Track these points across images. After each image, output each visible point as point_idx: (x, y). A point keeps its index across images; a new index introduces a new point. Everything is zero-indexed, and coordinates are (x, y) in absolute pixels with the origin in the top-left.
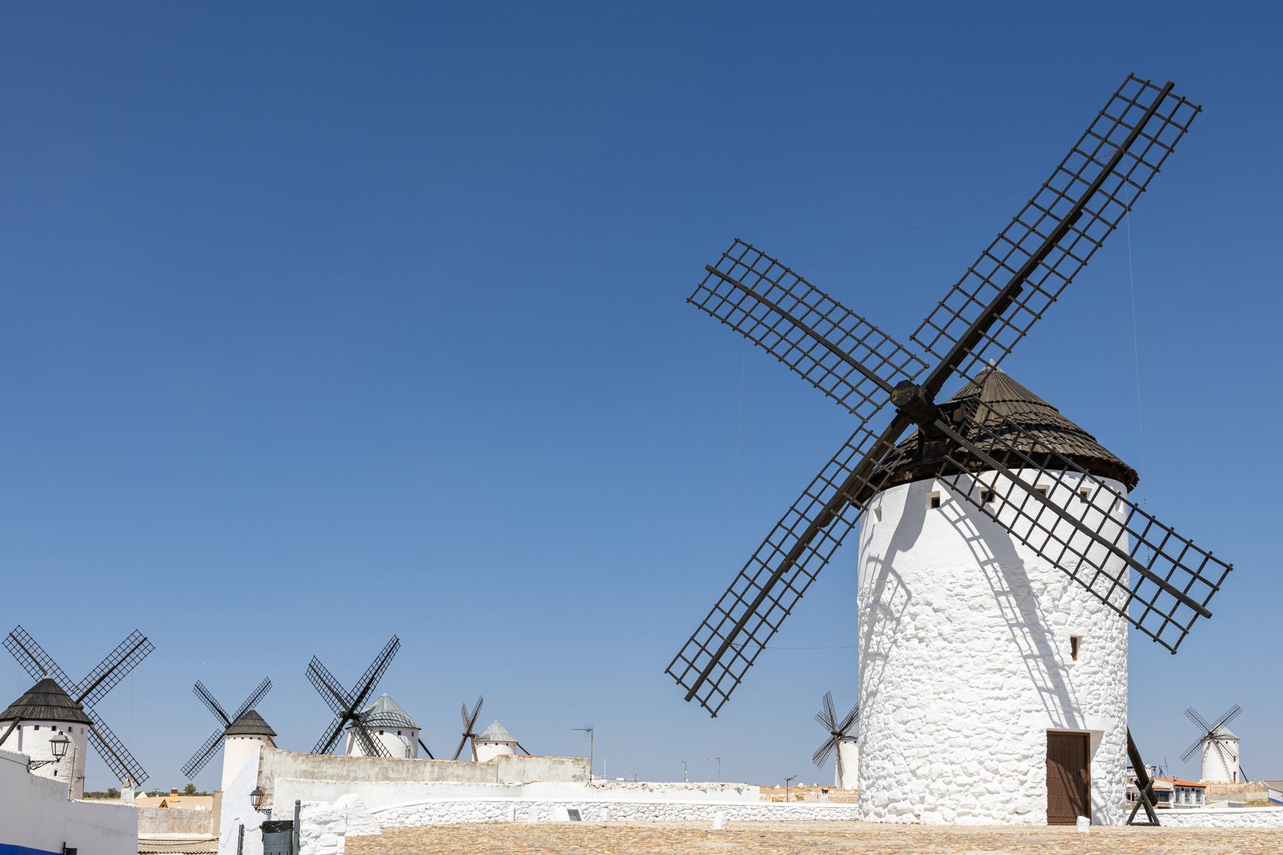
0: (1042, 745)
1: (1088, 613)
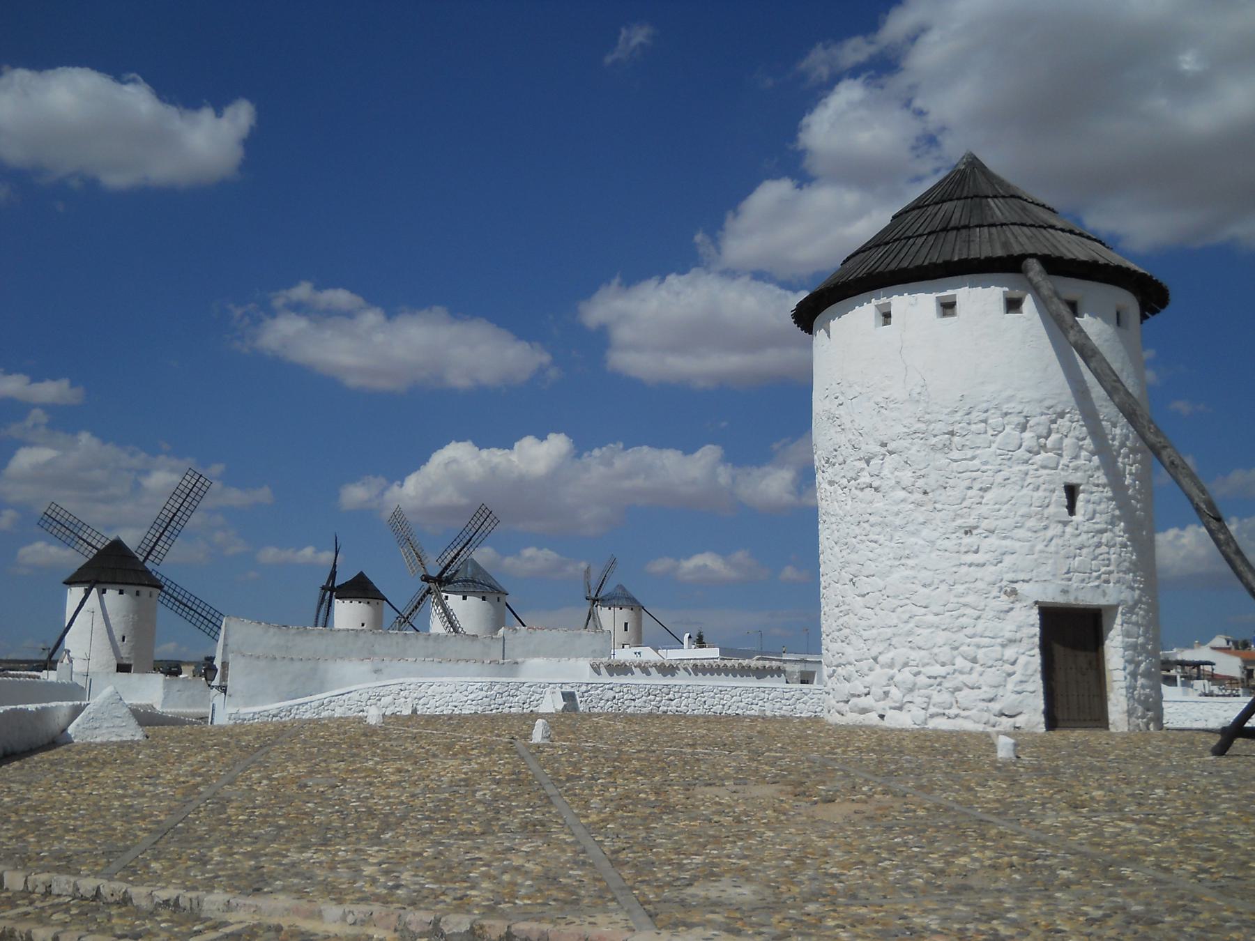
0: (1033, 625)
1: (1086, 453)
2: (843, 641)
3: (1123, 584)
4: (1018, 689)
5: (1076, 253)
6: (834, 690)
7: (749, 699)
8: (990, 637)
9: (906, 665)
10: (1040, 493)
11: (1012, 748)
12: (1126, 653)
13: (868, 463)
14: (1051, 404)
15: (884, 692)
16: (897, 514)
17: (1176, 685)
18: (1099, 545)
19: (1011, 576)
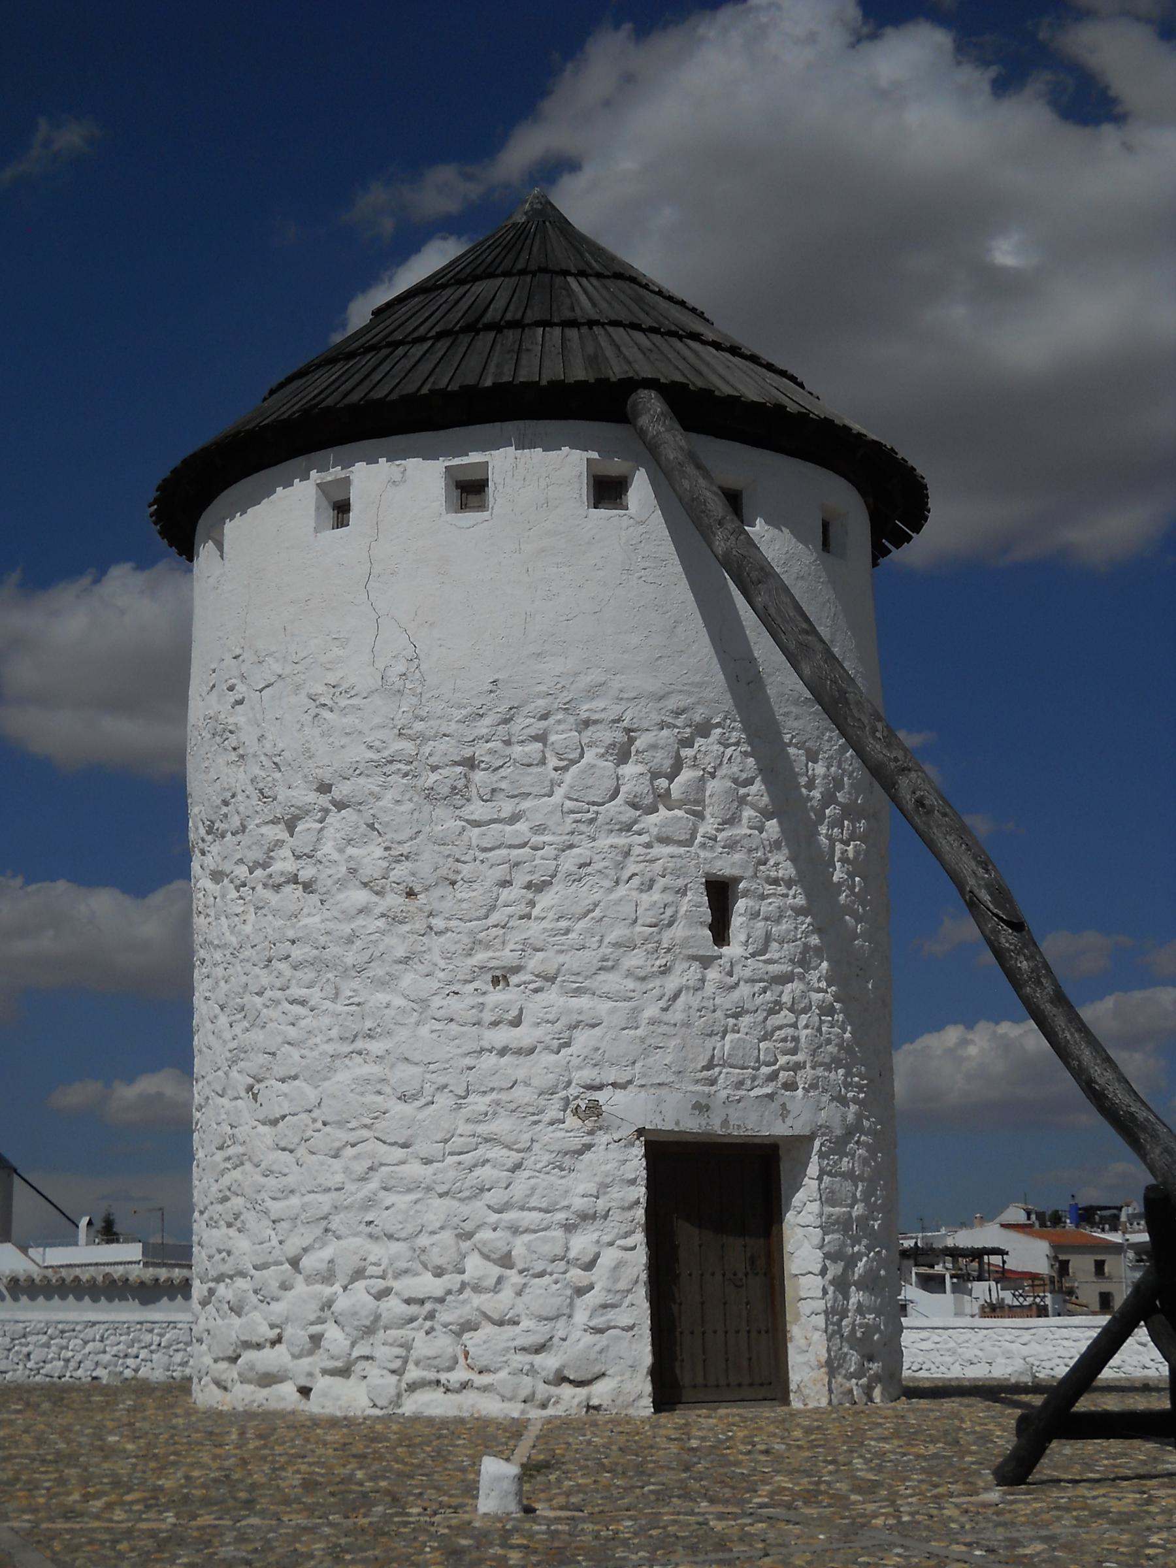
0: (633, 1182)
1: (753, 813)
2: (229, 1225)
3: (825, 1091)
4: (598, 1322)
5: (741, 387)
6: (208, 1331)
7: (121, 1347)
8: (540, 1210)
9: (359, 1274)
10: (656, 896)
11: (513, 1488)
12: (827, 1239)
13: (291, 827)
14: (682, 705)
15: (311, 1337)
16: (350, 941)
17: (945, 1292)
18: (775, 1008)
19: (587, 1075)
